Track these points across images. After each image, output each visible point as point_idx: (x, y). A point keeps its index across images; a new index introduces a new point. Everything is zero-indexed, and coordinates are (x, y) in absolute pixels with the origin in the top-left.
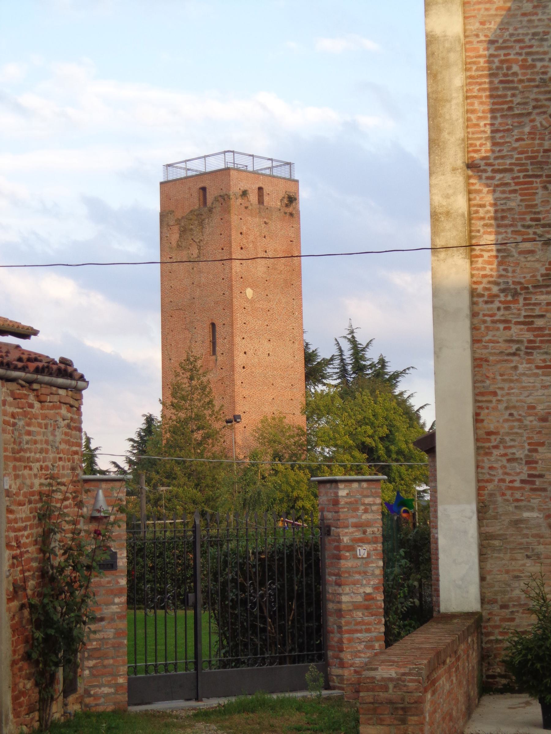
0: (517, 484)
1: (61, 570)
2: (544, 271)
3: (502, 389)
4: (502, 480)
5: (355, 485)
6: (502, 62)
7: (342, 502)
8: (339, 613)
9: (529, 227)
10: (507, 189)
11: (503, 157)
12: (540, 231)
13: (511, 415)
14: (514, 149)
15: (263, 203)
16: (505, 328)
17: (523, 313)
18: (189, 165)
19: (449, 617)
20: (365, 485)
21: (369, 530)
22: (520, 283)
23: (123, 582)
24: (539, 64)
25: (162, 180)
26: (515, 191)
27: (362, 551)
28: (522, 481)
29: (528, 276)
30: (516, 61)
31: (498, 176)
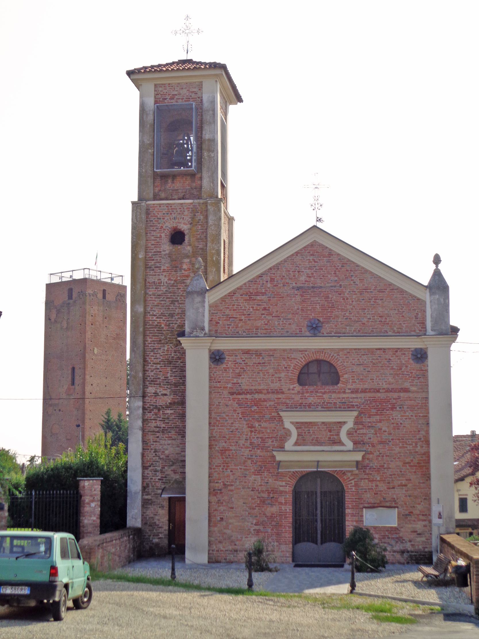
0: (157, 480)
1: (361, 618)
2: (170, 401)
3: (153, 445)
4: (152, 479)
5: (91, 481)
6: (158, 323)
7: (86, 488)
8: (84, 527)
9: (165, 385)
10: (158, 370)
11: (157, 359)
12: (169, 386)
13: (156, 454)
14: (161, 356)
15: (105, 299)
16: (155, 422)
17: (162, 417)
18: (63, 274)
19: (130, 528)
20: (95, 481)
21: (96, 498)
22: (161, 406)
23: (7, 514)
24: (171, 325)
25: (48, 283)
26: (161, 371)
27: (93, 505)
28: (159, 479)
29: (164, 403)
30: (163, 323)
31: (155, 365)
